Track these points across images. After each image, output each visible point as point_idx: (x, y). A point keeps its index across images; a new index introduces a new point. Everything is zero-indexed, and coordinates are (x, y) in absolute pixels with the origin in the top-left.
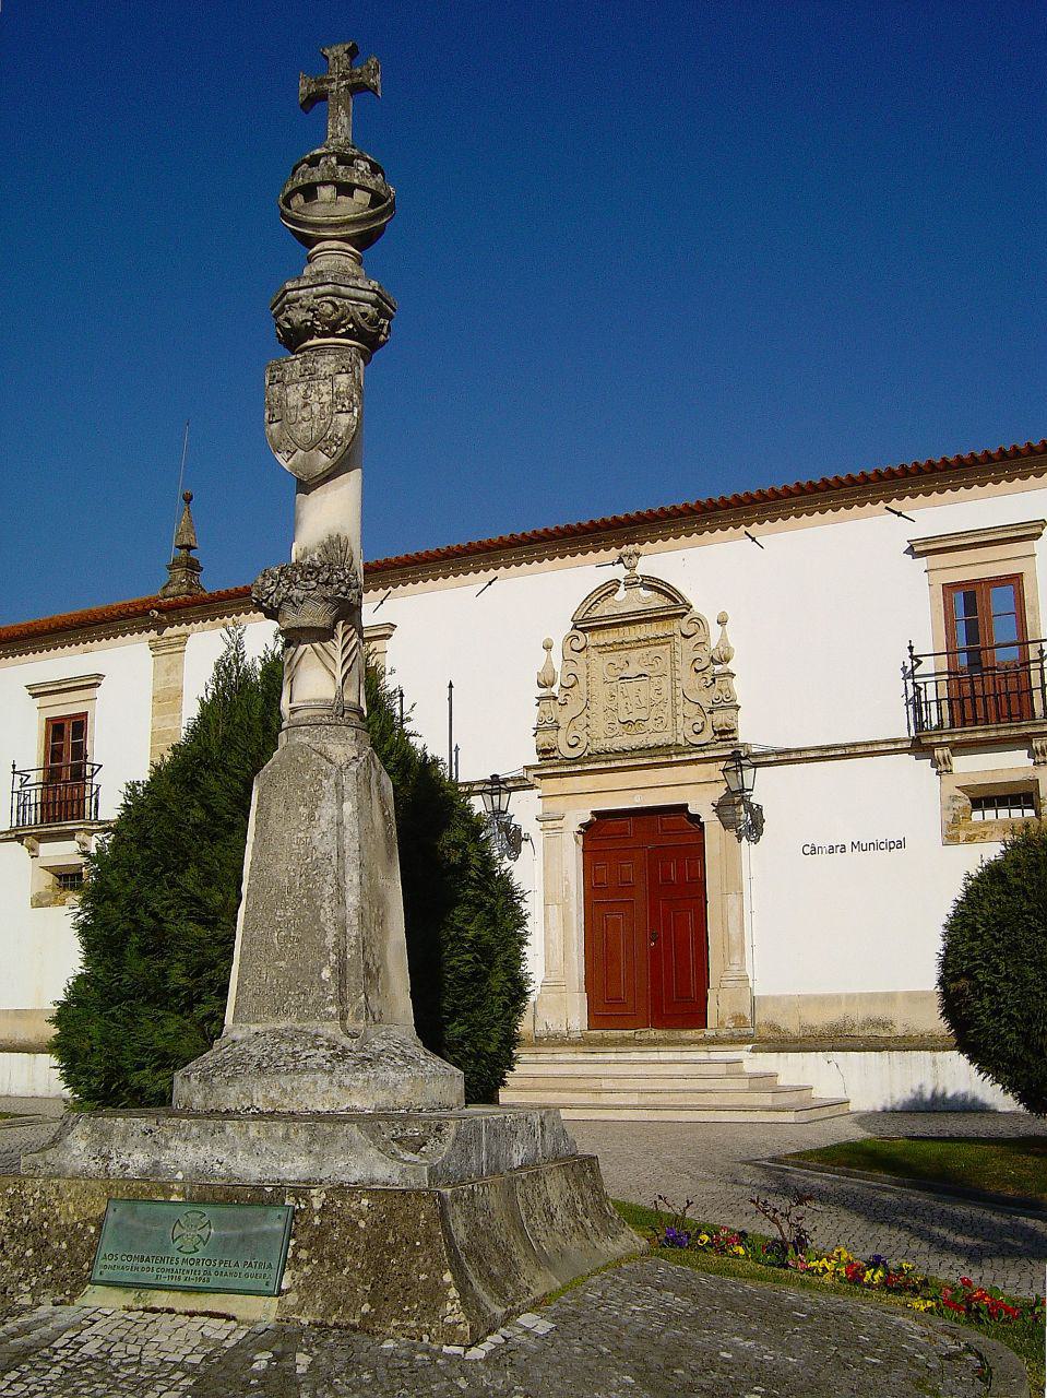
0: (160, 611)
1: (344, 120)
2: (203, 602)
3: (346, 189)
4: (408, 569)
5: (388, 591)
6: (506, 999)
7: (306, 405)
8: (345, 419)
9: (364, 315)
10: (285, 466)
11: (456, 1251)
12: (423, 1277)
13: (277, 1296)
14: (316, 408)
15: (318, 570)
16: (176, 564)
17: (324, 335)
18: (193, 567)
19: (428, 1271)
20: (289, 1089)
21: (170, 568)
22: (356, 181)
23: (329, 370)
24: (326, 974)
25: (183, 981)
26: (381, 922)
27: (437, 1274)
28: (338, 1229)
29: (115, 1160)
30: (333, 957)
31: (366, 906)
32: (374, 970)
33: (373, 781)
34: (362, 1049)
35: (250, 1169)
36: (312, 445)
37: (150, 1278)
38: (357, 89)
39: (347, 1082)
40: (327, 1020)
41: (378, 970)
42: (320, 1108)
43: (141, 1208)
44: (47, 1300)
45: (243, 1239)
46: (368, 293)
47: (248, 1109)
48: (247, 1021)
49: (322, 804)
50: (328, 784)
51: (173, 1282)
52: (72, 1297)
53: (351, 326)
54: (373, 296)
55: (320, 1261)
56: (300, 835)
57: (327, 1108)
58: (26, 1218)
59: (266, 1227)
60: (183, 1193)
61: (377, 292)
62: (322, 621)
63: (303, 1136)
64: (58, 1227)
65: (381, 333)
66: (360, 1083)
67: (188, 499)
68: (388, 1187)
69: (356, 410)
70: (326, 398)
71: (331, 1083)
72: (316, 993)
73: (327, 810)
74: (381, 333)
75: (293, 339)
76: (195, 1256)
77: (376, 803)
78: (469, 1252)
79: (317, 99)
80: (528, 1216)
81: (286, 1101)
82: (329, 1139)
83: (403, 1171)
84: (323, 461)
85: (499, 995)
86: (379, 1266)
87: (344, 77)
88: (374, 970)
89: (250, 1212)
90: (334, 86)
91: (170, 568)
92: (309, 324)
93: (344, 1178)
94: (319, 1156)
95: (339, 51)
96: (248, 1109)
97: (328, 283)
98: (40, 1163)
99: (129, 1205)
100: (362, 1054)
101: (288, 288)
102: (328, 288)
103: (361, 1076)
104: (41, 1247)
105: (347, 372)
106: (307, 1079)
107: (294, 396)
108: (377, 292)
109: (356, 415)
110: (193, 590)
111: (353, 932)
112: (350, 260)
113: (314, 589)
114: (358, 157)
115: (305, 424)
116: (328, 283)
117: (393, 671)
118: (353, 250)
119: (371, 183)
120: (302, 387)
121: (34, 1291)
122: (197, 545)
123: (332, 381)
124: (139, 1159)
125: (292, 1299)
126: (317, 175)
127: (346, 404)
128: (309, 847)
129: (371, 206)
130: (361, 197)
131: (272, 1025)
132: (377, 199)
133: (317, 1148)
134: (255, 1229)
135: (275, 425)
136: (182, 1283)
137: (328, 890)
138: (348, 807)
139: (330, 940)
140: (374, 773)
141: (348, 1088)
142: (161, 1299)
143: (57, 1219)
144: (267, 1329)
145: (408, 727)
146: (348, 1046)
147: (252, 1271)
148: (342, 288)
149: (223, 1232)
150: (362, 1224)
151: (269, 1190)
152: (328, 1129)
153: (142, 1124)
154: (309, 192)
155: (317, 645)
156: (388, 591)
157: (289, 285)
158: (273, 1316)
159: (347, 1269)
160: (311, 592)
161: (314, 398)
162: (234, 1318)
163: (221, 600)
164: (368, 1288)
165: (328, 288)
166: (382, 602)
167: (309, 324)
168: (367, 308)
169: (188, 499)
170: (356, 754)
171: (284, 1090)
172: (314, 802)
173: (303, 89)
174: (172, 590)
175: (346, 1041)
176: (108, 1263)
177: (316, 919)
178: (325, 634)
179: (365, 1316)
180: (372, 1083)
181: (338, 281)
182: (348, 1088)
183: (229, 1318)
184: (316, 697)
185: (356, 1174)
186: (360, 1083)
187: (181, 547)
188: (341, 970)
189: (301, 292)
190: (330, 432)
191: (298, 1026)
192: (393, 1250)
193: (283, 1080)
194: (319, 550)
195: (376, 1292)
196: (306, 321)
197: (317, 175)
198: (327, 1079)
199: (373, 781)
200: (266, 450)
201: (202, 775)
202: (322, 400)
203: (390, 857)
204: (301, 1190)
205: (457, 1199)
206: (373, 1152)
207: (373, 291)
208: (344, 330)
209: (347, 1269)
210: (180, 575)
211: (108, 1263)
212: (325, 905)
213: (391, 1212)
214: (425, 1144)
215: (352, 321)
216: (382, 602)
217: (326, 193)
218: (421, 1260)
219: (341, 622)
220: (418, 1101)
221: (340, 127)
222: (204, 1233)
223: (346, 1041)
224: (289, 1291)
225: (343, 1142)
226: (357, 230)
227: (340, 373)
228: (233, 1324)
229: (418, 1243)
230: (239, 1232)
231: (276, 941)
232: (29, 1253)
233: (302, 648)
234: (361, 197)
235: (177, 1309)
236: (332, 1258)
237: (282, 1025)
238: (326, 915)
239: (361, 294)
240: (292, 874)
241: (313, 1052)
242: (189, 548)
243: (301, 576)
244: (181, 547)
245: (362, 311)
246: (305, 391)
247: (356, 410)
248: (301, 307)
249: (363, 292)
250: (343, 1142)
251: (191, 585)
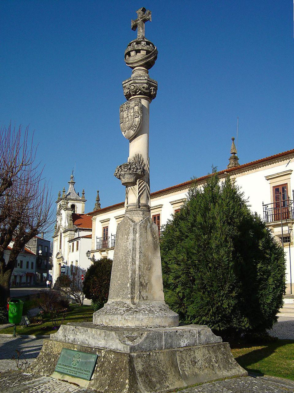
0: (227, 172)
1: (141, 31)
2: (239, 168)
3: (138, 51)
4: (289, 155)
5: (290, 160)
6: (274, 286)
7: (128, 117)
8: (137, 119)
9: (144, 87)
10: (124, 135)
11: (135, 374)
12: (122, 380)
13: (90, 381)
14: (130, 117)
15: (128, 165)
16: (231, 158)
17: (134, 95)
18: (236, 159)
19: (123, 379)
20: (111, 319)
21: (229, 159)
22: (140, 48)
23: (133, 105)
24: (128, 285)
25: (172, 281)
26: (149, 269)
27: (125, 380)
28: (106, 363)
29: (67, 337)
30: (130, 280)
31: (142, 265)
32: (145, 284)
33: (148, 227)
34: (136, 308)
35: (93, 343)
36: (129, 128)
37: (65, 371)
38: (145, 21)
39: (127, 318)
40: (128, 299)
41: (147, 284)
42: (119, 326)
43: (68, 351)
44: (46, 374)
45: (86, 363)
46: (144, 81)
47: (102, 325)
48: (111, 299)
49: (130, 234)
50: (131, 228)
51: (70, 373)
52: (50, 374)
53: (140, 91)
54: (146, 81)
55: (101, 372)
56: (125, 244)
57: (121, 326)
58: (48, 351)
59: (91, 360)
60: (77, 348)
61: (147, 80)
62: (132, 180)
63: (103, 334)
64: (53, 355)
65: (152, 92)
66: (130, 319)
67: (233, 139)
68: (121, 352)
69: (140, 116)
70: (132, 114)
71: (122, 318)
72: (126, 291)
73: (131, 236)
74: (152, 92)
75: (128, 96)
76: (76, 366)
77: (149, 233)
78: (141, 374)
79: (135, 27)
80: (181, 363)
81: (110, 323)
82: (109, 336)
83: (124, 347)
84: (132, 132)
85: (272, 285)
86: (113, 375)
87: (141, 18)
88: (145, 284)
89: (89, 355)
90: (139, 22)
91: (229, 159)
92: (129, 93)
93: (111, 347)
94: (107, 340)
95: (140, 11)
96: (102, 325)
97: (132, 80)
98: (54, 337)
99: (66, 350)
100: (136, 310)
101: (123, 83)
102: (132, 82)
103: (131, 316)
104: (49, 360)
105: (137, 105)
106: (116, 317)
107: (125, 116)
108: (147, 80)
109: (140, 118)
110: (236, 165)
111: (137, 272)
112: (142, 72)
113: (126, 171)
114: (142, 41)
115: (127, 123)
116: (132, 80)
117: (241, 187)
118: (145, 69)
119: (145, 48)
120: (127, 111)
121: (44, 372)
122: (237, 153)
123: (134, 109)
124: (71, 337)
125: (92, 382)
126: (130, 48)
127: (137, 115)
128: (126, 246)
129: (146, 54)
130: (143, 53)
131: (116, 300)
132: (148, 52)
133: (106, 338)
134: (89, 361)
135: (122, 124)
136: (71, 374)
137: (130, 260)
138: (138, 235)
139: (130, 275)
140: (149, 224)
141: (127, 320)
142: (67, 378)
143: (53, 352)
144: (83, 390)
145: (247, 204)
146: (132, 307)
147: (85, 372)
148: (136, 81)
149: (82, 360)
150: (112, 362)
151: (94, 349)
152: (109, 333)
153: (72, 327)
154: (129, 54)
155: (132, 187)
156: (290, 160)
157: (123, 83)
158: (86, 387)
159: (106, 375)
160: (126, 172)
161: (129, 114)
162: (79, 386)
163: (243, 167)
164: (109, 381)
165: (132, 82)
166: (288, 164)
167: (129, 93)
168: (145, 85)
169: (233, 139)
170: (142, 219)
171: (110, 320)
172: (128, 234)
173: (132, 24)
174: (230, 166)
175: (132, 306)
176: (59, 366)
177: (127, 269)
178: (134, 184)
179: (106, 390)
180: (134, 319)
181: (135, 79)
182: (127, 320)
183: (78, 385)
184: (132, 203)
185: (113, 347)
186: (130, 319)
187: (232, 153)
188: (133, 285)
189: (126, 84)
190: (133, 124)
191: (122, 300)
192: (117, 371)
193: (110, 317)
194: (133, 159)
195: (110, 383)
196: (128, 92)
197: (130, 48)
198: (121, 317)
199: (148, 227)
200: (119, 131)
201: (180, 222)
202: (131, 115)
203: (155, 249)
204: (99, 350)
205: (139, 356)
206: (117, 340)
207: (146, 80)
208: (138, 93)
209: (106, 375)
210: (232, 161)
211: (59, 366)
212: (129, 265)
213: (118, 359)
214: (136, 339)
215: (140, 90)
216: (288, 164)
217: (133, 53)
218: (123, 375)
219: (138, 180)
220: (150, 324)
221: (140, 33)
222: (78, 360)
223: (132, 306)
224: (93, 379)
225: (111, 337)
226: (144, 62)
227: (135, 106)
228: (78, 387)
229: (123, 370)
230: (85, 361)
231: (118, 275)
232: (47, 361)
233: (129, 188)
234: (143, 53)
235: (69, 382)
236: (104, 371)
237: (118, 300)
238: (129, 268)
239: (142, 81)
240: (122, 255)
241: (122, 308)
242: (235, 153)
243: (124, 168)
244: (232, 153)
245: (143, 86)
246: (127, 113)
247: (140, 116)
248: (127, 88)
249: (143, 81)
250: (111, 337)
251: (235, 164)
